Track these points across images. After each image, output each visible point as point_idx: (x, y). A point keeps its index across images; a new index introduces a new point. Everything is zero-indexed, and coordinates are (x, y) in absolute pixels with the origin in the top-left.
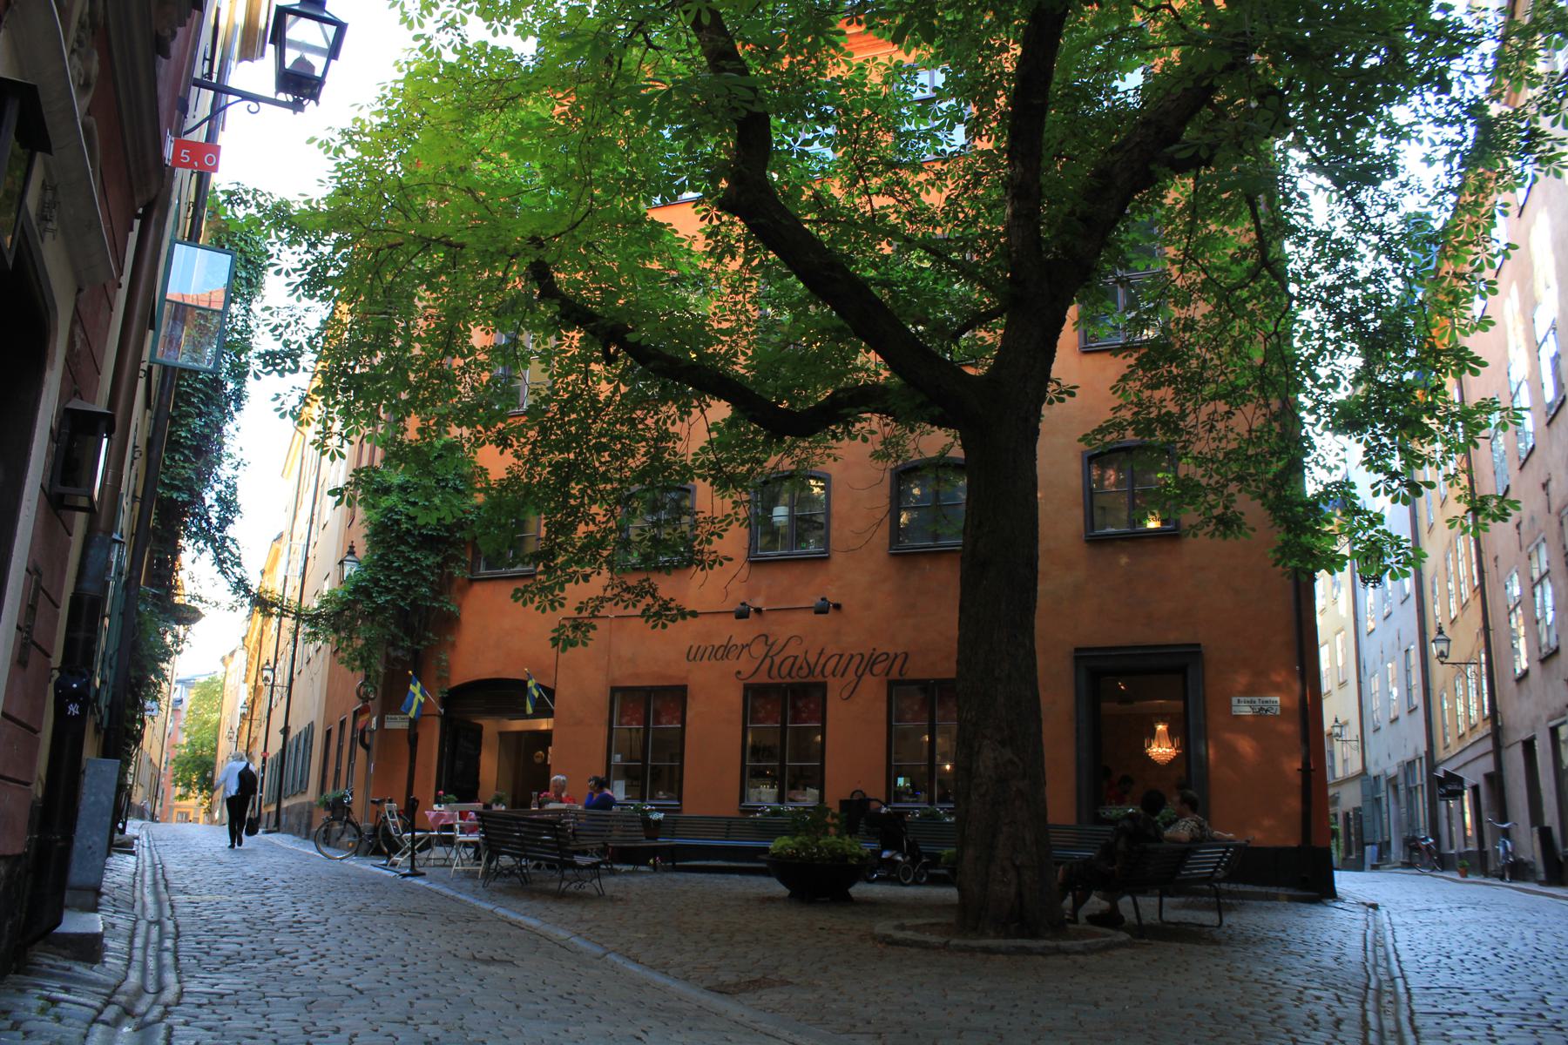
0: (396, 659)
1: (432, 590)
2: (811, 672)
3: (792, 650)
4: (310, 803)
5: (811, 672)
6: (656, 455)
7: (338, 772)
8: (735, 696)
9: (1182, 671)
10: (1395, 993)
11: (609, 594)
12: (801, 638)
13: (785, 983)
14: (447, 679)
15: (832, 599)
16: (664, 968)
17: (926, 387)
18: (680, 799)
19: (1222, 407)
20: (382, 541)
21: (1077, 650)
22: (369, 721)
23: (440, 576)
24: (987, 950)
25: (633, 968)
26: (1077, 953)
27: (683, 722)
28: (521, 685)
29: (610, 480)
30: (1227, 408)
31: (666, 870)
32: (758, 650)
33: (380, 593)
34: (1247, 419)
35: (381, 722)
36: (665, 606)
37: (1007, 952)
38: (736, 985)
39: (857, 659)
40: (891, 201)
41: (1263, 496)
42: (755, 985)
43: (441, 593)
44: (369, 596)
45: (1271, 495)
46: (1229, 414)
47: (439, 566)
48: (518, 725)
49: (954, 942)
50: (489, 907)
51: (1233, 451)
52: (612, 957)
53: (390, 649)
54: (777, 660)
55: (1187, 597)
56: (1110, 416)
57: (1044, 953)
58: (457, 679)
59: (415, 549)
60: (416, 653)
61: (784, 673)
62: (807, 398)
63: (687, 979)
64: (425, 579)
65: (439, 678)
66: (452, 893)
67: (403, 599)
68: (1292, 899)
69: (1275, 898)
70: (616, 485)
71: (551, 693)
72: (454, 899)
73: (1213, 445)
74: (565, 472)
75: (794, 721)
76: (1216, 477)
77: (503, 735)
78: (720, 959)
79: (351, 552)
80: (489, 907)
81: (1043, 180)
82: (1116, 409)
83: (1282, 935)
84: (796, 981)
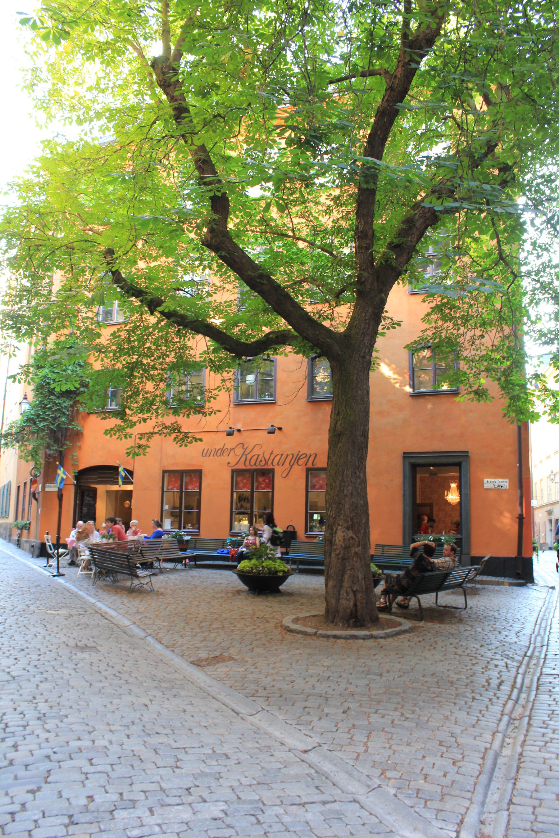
0: (50, 455)
1: (68, 419)
2: (266, 463)
3: (256, 451)
4: (11, 524)
5: (266, 463)
6: (180, 357)
7: (23, 509)
8: (227, 476)
9: (459, 465)
10: (539, 658)
11: (156, 430)
12: (261, 447)
13: (231, 658)
14: (77, 466)
15: (277, 425)
16: (171, 647)
17: (312, 337)
18: (199, 528)
19: (478, 332)
20: (41, 393)
21: (404, 453)
22: (37, 487)
23: (72, 412)
24: (336, 637)
25: (158, 646)
26: (381, 638)
27: (200, 488)
28: (116, 468)
29: (156, 369)
30: (481, 333)
31: (191, 567)
32: (239, 451)
33: (40, 422)
34: (492, 337)
35: (43, 488)
36: (186, 435)
37: (346, 638)
38: (207, 659)
39: (290, 457)
40: (303, 220)
41: (499, 379)
42: (217, 660)
43: (73, 420)
44: (35, 423)
45: (503, 379)
46: (482, 336)
47: (72, 406)
48: (115, 488)
49: (320, 632)
50: (93, 600)
51: (483, 356)
52: (149, 639)
53: (47, 450)
54: (249, 457)
55: (461, 425)
56: (421, 334)
57: (364, 638)
58: (83, 466)
59: (58, 397)
60: (61, 452)
61: (275, 463)
62: (255, 336)
63: (182, 656)
64: (64, 413)
65: (73, 465)
66: (76, 590)
67: (53, 424)
68: (511, 584)
69: (502, 584)
70: (159, 371)
71: (131, 473)
72: (76, 596)
73: (473, 353)
74: (132, 368)
75: (257, 489)
76: (475, 370)
77: (107, 492)
78: (202, 641)
79: (25, 398)
80: (93, 600)
81: (375, 227)
82: (424, 331)
83: (496, 614)
84: (236, 657)
